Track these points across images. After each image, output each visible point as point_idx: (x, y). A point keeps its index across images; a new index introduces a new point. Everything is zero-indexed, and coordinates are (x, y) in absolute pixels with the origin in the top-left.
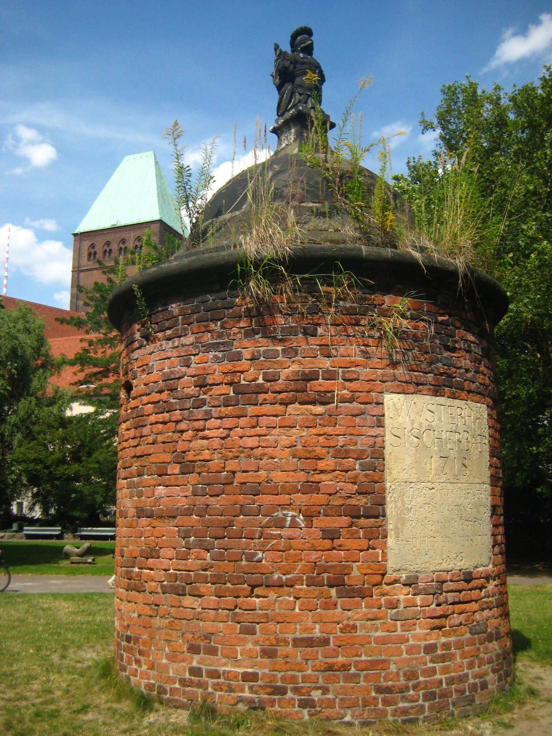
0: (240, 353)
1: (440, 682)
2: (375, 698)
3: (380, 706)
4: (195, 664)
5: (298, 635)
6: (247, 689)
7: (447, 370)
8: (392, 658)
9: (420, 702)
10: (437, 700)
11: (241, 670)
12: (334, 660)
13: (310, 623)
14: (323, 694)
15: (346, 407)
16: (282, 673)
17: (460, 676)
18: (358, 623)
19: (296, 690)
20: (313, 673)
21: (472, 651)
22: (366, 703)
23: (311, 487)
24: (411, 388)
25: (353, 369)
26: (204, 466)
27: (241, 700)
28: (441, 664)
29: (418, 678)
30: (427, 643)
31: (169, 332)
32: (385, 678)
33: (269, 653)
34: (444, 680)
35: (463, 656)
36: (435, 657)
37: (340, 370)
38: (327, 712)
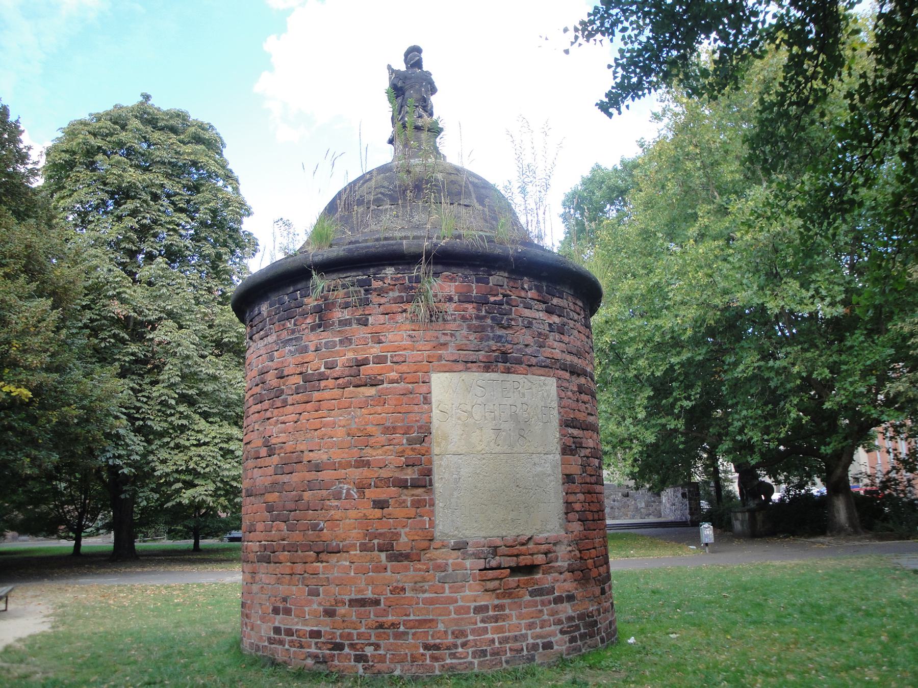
0: (306, 347)
1: (493, 641)
2: (423, 655)
3: (428, 662)
4: (277, 624)
5: (353, 596)
6: (313, 645)
9: (470, 659)
10: (488, 657)
11: (308, 629)
12: (384, 619)
13: (363, 585)
14: (376, 650)
15: (395, 388)
18: (406, 585)
19: (352, 646)
21: (533, 612)
23: (362, 463)
24: (460, 366)
26: (282, 448)
27: (310, 655)
30: (478, 604)
31: (262, 333)
32: (432, 636)
33: (330, 613)
37: (389, 354)
38: (379, 666)
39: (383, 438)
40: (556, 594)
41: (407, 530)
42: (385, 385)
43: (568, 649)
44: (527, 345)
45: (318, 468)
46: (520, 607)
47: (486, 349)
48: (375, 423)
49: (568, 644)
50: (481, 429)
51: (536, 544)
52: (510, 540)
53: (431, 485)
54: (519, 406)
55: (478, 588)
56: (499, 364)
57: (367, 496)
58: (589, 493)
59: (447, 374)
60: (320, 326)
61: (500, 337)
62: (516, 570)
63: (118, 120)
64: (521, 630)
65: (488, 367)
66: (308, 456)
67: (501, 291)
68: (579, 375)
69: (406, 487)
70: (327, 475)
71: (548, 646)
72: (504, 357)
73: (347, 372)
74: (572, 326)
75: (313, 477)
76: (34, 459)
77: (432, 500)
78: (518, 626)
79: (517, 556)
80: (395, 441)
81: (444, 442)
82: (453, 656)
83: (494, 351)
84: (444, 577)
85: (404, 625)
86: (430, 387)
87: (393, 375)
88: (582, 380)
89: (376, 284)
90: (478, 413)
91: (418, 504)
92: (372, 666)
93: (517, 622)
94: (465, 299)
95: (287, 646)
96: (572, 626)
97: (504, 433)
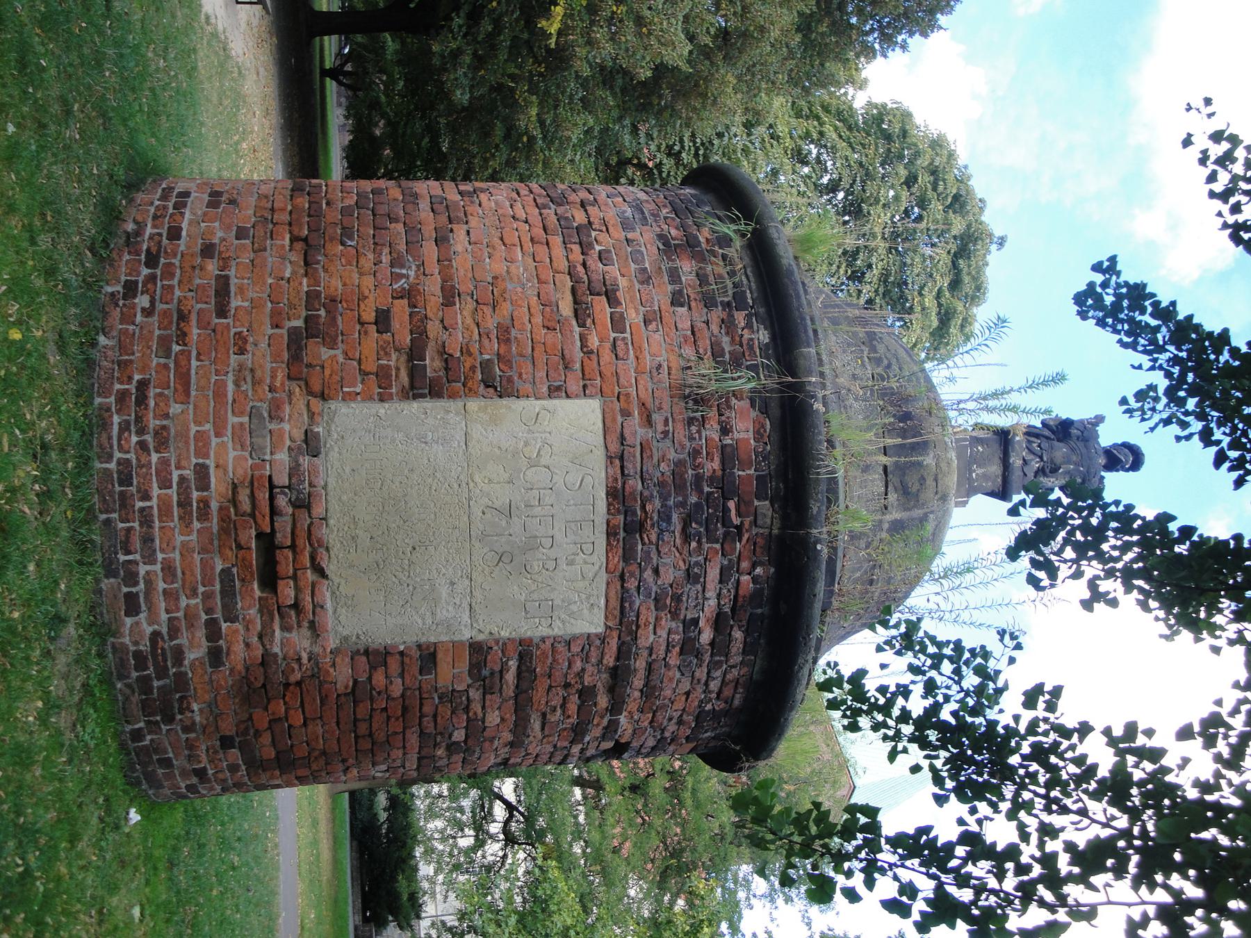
0: (633, 229)
2: (130, 378)
3: (117, 386)
5: (234, 281)
7: (652, 519)
8: (191, 406)
9: (118, 455)
10: (118, 488)
11: (185, 225)
12: (194, 322)
13: (251, 294)
14: (143, 309)
15: (573, 343)
16: (177, 264)
17: (153, 540)
19: (152, 279)
20: (176, 297)
21: (193, 574)
22: (123, 365)
23: (450, 296)
24: (615, 447)
25: (631, 352)
27: (140, 226)
28: (175, 498)
29: (157, 451)
30: (212, 470)
32: (160, 395)
33: (208, 250)
34: (148, 504)
35: (186, 550)
36: (188, 487)
37: (628, 335)
39: (491, 323)
40: (224, 626)
41: (341, 359)
42: (577, 329)
43: (124, 647)
44: (656, 571)
45: (441, 240)
46: (203, 550)
47: (646, 493)
48: (516, 313)
49: (132, 648)
50: (510, 482)
51: (313, 585)
52: (323, 532)
53: (415, 397)
54: (553, 553)
55: (240, 472)
56: (622, 517)
57: (396, 301)
58: (405, 709)
59: (601, 425)
60: (666, 243)
61: (668, 519)
62: (267, 542)
63: (959, 202)
64: (162, 551)
65: (616, 495)
66: (460, 231)
67: (747, 521)
68: (611, 690)
69: (411, 358)
70: (430, 250)
71: (132, 605)
72: (635, 528)
73: (594, 277)
74: (697, 674)
75: (426, 235)
76: (456, 54)
77: (391, 397)
78: (169, 545)
79: (293, 547)
80: (486, 342)
81: (486, 417)
82: (125, 427)
83: (643, 507)
84: (261, 416)
85: (182, 352)
86: (577, 396)
87: (594, 342)
88: (603, 701)
89: (740, 317)
90: (537, 476)
91: (383, 376)
92: (117, 305)
93: (178, 544)
94: (728, 456)
95: (157, 203)
96: (165, 660)
97: (504, 523)
